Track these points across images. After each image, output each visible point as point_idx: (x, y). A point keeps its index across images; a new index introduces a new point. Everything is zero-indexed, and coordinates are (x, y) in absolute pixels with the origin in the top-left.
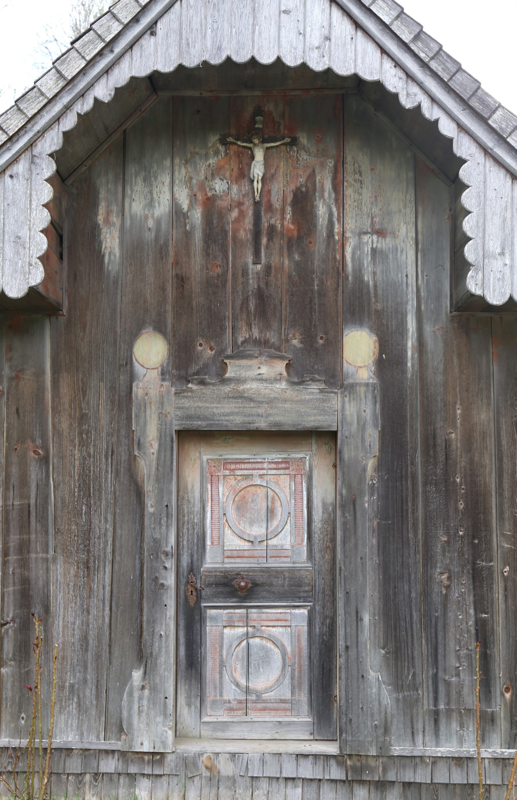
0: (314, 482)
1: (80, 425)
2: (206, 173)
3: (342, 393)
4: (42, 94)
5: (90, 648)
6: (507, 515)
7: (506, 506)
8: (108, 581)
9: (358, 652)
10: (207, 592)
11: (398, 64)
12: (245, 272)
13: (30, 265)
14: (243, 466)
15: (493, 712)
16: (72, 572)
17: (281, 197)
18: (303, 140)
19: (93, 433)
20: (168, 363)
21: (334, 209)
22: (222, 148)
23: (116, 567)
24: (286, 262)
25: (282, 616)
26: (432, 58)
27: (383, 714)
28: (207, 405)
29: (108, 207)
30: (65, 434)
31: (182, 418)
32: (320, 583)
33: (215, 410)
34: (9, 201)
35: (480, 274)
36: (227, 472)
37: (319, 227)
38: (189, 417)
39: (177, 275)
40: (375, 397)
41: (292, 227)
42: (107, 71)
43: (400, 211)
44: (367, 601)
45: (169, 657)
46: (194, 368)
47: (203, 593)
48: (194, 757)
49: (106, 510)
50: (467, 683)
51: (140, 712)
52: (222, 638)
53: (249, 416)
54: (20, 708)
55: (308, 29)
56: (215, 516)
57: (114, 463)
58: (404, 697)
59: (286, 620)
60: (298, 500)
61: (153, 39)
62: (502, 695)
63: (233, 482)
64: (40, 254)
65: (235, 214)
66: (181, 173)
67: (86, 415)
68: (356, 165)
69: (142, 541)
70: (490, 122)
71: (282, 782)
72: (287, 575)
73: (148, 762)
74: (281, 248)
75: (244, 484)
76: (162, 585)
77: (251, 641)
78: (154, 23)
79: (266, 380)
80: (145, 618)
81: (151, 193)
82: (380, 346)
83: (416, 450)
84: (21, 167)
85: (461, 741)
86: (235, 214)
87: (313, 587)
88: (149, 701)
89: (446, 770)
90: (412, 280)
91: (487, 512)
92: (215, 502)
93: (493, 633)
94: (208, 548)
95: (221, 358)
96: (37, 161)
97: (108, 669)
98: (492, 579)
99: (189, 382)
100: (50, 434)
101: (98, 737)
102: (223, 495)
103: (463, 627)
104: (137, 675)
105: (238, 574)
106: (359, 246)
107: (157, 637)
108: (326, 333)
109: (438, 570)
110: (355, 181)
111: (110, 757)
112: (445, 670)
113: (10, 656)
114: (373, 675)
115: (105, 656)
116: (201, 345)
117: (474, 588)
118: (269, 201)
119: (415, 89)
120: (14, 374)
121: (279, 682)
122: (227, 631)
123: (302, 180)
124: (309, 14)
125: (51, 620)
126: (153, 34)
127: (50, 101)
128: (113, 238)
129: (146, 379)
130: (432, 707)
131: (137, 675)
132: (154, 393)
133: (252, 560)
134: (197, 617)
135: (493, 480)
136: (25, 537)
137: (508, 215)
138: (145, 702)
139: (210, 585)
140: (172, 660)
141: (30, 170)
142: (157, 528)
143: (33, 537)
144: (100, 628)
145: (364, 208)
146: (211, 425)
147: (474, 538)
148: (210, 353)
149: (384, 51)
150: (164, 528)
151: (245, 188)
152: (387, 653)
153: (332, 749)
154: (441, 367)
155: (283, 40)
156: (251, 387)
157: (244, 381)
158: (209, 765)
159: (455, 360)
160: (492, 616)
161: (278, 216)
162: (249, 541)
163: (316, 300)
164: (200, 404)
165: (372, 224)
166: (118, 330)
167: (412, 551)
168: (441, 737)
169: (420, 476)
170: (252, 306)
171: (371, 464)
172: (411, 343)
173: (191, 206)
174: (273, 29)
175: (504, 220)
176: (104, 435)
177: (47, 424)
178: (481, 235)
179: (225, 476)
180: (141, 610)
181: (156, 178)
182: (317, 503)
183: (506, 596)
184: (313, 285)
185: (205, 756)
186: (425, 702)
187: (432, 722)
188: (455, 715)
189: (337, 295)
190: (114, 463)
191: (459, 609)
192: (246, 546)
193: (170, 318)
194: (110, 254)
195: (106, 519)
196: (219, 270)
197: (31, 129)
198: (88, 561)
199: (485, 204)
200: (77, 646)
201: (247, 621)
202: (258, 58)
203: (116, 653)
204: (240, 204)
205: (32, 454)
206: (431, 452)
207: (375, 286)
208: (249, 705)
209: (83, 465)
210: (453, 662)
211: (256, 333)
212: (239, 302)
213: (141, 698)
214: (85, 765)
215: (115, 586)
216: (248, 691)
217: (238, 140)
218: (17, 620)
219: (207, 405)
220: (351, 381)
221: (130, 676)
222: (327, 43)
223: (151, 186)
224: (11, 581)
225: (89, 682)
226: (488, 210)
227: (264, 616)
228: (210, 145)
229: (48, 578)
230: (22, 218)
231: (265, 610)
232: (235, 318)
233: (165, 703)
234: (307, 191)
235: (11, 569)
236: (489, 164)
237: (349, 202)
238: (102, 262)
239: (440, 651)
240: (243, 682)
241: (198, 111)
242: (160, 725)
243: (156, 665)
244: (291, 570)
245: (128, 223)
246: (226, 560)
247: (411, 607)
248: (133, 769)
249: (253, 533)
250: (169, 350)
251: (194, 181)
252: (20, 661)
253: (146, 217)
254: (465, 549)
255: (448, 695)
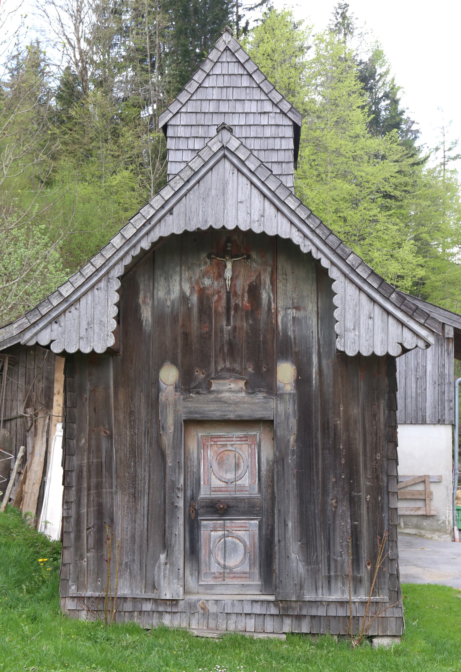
0: (262, 449)
1: (130, 417)
2: (199, 275)
3: (276, 399)
4: (114, 246)
5: (136, 542)
6: (369, 466)
7: (368, 461)
8: (146, 504)
9: (285, 543)
10: (201, 511)
11: (299, 230)
12: (222, 331)
13: (108, 336)
14: (221, 439)
15: (361, 577)
16: (126, 499)
17: (242, 288)
18: (254, 255)
19: (137, 421)
20: (179, 382)
21: (272, 295)
22: (208, 261)
23: (150, 496)
24: (245, 325)
25: (244, 525)
26: (317, 227)
27: (299, 577)
28: (201, 405)
29: (145, 294)
30: (122, 422)
31: (187, 413)
32: (265, 506)
33: (205, 409)
34: (96, 302)
35: (343, 340)
36: (212, 443)
37: (263, 305)
38: (191, 412)
39: (184, 332)
40: (294, 401)
41: (248, 305)
42: (147, 233)
43: (308, 296)
44: (290, 515)
45: (180, 546)
46: (193, 385)
47: (199, 512)
48: (195, 602)
49: (145, 464)
50: (346, 560)
51: (164, 577)
52: (210, 537)
53: (224, 411)
54: (98, 575)
55: (253, 211)
56: (206, 468)
57: (149, 438)
58: (311, 568)
59: (246, 527)
60: (253, 459)
61: (171, 217)
62: (366, 567)
63: (216, 449)
64: (112, 330)
65: (216, 297)
66: (186, 275)
67: (134, 411)
68: (284, 270)
69: (165, 482)
70: (347, 261)
71: (243, 616)
72: (247, 501)
73: (169, 605)
74: (242, 317)
75: (222, 450)
76: (176, 506)
77: (227, 539)
78: (172, 208)
79: (233, 392)
80: (167, 525)
81: (169, 287)
82: (298, 372)
83: (318, 430)
84: (102, 284)
85: (343, 592)
86: (216, 297)
87: (262, 508)
88: (169, 571)
89: (335, 609)
90: (315, 335)
91: (357, 465)
92: (206, 460)
93: (361, 532)
94: (202, 486)
95: (209, 379)
96: (111, 281)
97: (147, 554)
98: (360, 502)
99: (190, 392)
100: (113, 422)
101: (141, 591)
102: (210, 456)
103: (345, 529)
104: (163, 557)
105: (219, 501)
106: (285, 316)
107: (174, 535)
108: (267, 365)
109: (330, 498)
110: (283, 279)
111: (148, 602)
112: (334, 553)
113: (92, 546)
114: (293, 556)
115: (145, 546)
116: (197, 372)
117: (350, 508)
118: (235, 290)
119: (308, 243)
120: (92, 389)
121: (242, 562)
122: (213, 533)
123: (254, 278)
124: (253, 203)
125: (114, 526)
126: (171, 214)
127: (118, 250)
128: (148, 312)
129: (166, 391)
130: (327, 574)
131: (163, 557)
132: (171, 399)
133: (227, 493)
134: (196, 526)
135: (361, 447)
136: (100, 480)
137: (357, 309)
138: (167, 572)
139: (203, 507)
140: (182, 548)
141: (107, 285)
142: (174, 474)
143: (104, 480)
144: (142, 531)
145: (288, 294)
146: (203, 417)
147: (350, 480)
148: (202, 376)
149: (292, 223)
150: (177, 474)
151: (222, 283)
152: (302, 544)
153: (272, 598)
154: (332, 383)
155: (240, 217)
156: (226, 395)
157: (221, 392)
158: (203, 607)
159: (339, 379)
160: (360, 523)
161: (240, 299)
162: (225, 482)
163: (262, 346)
164: (197, 405)
165: (293, 303)
166: (151, 363)
167: (316, 487)
168: (332, 591)
169: (320, 445)
170: (226, 349)
171: (292, 438)
172: (314, 370)
173: (191, 293)
174: (234, 211)
175: (355, 312)
176: (143, 422)
177: (111, 417)
178: (343, 319)
179: (211, 445)
180: (165, 521)
181: (172, 278)
182: (263, 460)
183: (368, 512)
184: (260, 338)
185: (201, 601)
186: (323, 571)
187: (327, 582)
188: (340, 579)
189: (273, 343)
190: (149, 438)
191: (342, 519)
192: (223, 485)
193: (180, 356)
194: (146, 321)
195: (145, 469)
196: (207, 329)
197: (108, 265)
198: (135, 493)
199: (345, 303)
200: (129, 541)
201: (224, 528)
202: (226, 226)
203: (151, 544)
204: (219, 292)
205: (103, 433)
206: (326, 432)
207: (295, 338)
208: (225, 575)
209: (131, 439)
210: (338, 549)
211: (228, 365)
212: (218, 347)
213: (165, 570)
214: (135, 606)
215: (150, 507)
216: (225, 567)
217: (217, 256)
218: (96, 527)
219: (201, 405)
220: (281, 392)
221: (159, 557)
222: (262, 218)
223: (169, 282)
224: (92, 504)
225: (136, 561)
226: (347, 306)
227: (234, 525)
228: (202, 259)
229: (112, 503)
230: (103, 311)
231: (234, 521)
232: (216, 357)
233: (178, 572)
234: (256, 285)
235: (92, 498)
236: (347, 282)
237: (279, 291)
238: (142, 325)
239: (332, 543)
240: (222, 562)
241: (195, 240)
242: (176, 584)
243: (173, 551)
244: (249, 499)
245: (156, 303)
246: (212, 493)
247: (315, 518)
248: (161, 609)
249: (227, 477)
250: (179, 374)
251: (193, 279)
252: (98, 549)
253: (166, 300)
254: (345, 486)
255: (336, 567)
